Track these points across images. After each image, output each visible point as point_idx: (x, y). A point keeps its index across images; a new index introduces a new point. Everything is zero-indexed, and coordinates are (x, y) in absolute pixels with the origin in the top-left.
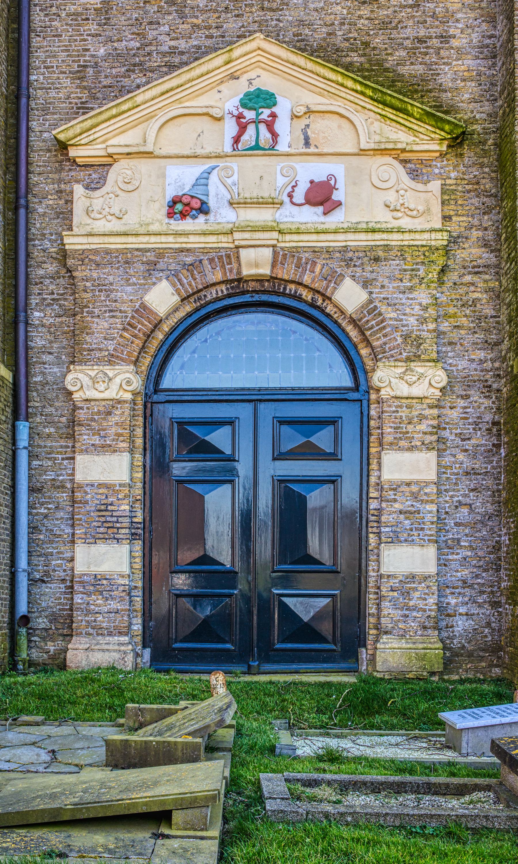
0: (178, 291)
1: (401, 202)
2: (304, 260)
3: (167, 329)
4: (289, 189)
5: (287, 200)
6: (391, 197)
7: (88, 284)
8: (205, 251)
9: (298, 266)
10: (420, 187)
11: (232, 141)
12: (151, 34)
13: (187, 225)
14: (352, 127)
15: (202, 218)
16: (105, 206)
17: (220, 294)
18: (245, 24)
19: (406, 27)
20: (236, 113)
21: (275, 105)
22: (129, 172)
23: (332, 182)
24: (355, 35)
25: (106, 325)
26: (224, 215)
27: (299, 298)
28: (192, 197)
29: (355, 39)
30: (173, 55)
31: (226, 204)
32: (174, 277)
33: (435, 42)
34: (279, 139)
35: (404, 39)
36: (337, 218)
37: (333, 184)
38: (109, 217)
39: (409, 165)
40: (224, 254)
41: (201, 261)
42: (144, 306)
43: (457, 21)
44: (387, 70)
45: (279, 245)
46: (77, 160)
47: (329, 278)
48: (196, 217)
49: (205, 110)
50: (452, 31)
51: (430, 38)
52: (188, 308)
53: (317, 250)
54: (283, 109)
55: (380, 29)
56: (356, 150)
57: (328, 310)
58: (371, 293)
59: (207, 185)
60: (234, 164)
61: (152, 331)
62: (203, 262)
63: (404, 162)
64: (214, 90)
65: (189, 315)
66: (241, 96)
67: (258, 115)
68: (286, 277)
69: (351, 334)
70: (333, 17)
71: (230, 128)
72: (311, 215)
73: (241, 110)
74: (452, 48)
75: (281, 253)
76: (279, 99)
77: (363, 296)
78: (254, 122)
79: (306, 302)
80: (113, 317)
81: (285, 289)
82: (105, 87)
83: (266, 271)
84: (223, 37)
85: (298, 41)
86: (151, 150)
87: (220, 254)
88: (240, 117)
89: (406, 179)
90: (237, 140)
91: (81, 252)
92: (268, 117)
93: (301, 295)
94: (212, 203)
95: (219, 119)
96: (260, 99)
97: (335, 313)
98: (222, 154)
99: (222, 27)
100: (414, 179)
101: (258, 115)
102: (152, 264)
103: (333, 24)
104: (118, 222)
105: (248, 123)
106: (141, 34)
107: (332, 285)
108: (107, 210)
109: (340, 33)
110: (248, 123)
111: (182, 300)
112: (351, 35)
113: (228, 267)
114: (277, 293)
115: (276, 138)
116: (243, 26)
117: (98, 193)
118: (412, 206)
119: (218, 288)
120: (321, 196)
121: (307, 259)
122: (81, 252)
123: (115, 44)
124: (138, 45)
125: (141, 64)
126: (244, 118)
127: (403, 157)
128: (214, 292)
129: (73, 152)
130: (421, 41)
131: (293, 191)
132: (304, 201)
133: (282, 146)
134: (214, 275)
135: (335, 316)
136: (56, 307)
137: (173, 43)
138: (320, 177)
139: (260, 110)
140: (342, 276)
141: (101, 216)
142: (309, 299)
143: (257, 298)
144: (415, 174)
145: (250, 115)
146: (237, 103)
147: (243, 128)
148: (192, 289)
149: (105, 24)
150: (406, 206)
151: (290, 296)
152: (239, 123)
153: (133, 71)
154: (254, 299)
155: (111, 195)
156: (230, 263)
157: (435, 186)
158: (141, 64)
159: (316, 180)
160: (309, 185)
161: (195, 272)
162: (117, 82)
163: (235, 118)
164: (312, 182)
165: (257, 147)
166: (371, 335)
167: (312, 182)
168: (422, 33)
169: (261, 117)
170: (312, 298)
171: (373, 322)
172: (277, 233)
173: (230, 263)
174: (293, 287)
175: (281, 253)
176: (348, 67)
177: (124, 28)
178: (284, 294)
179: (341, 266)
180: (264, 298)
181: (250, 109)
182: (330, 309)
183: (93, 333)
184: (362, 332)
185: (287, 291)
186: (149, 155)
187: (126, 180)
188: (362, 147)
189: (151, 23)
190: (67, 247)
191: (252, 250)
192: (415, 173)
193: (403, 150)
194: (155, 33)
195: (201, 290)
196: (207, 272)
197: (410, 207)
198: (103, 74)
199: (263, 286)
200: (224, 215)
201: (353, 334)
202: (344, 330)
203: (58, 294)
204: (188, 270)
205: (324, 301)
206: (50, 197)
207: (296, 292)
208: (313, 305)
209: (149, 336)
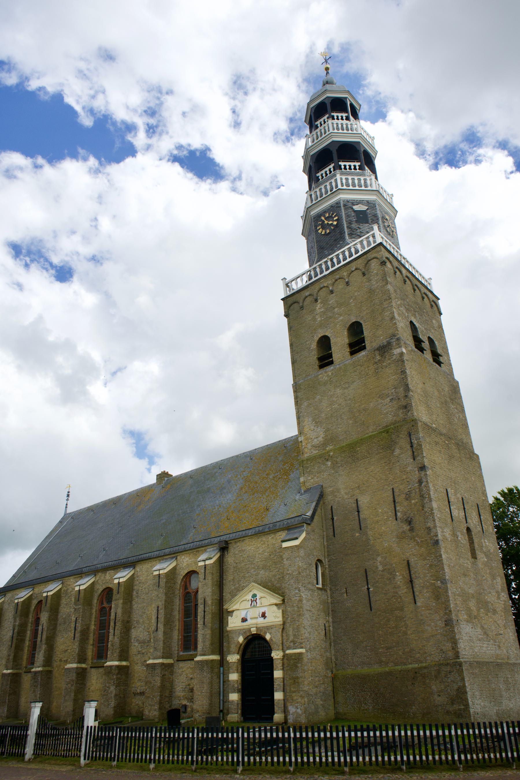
13: (245, 624)
102: (240, 632)
127: (276, 605)
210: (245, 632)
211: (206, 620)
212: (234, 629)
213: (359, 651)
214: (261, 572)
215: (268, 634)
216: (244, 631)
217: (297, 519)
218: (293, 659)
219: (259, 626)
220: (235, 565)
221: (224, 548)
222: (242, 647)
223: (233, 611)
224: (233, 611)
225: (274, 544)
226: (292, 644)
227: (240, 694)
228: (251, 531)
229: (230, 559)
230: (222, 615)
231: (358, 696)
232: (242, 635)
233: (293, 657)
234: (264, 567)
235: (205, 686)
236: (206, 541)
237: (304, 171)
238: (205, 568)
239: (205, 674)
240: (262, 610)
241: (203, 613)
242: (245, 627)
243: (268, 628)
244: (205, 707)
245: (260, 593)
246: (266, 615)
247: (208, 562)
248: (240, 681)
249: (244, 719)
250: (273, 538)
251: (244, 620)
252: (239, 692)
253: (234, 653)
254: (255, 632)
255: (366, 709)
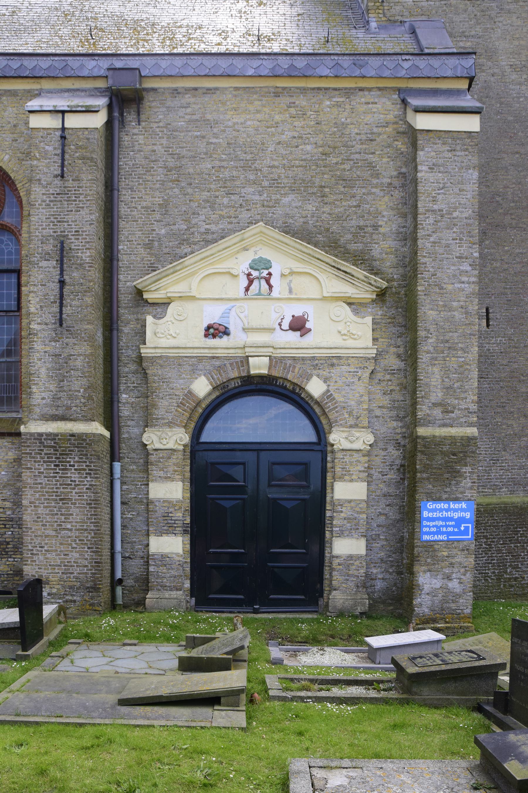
26: (237, 339)
72: (293, 337)
102: (195, 364)
210: (219, 369)
211: (67, 310)
212: (172, 353)
213: (506, 455)
214: (285, 200)
215: (315, 379)
216: (218, 363)
217: (453, 61)
218: (442, 453)
219: (280, 353)
220: (171, 163)
221: (125, 99)
222: (200, 410)
225: (345, 125)
226: (437, 412)
227: (188, 538)
228: (255, 63)
229: (139, 140)
230: (117, 311)
231: (499, 551)
232: (209, 375)
233: (445, 448)
234: (302, 187)
235: (74, 511)
236: (44, 63)
238: (63, 138)
239: (75, 476)
240: (298, 310)
241: (56, 286)
242: (220, 353)
244: (76, 571)
245: (284, 259)
246: (308, 325)
247: (73, 122)
248: (187, 504)
249: (197, 604)
250: (338, 105)
251: (215, 331)
252: (185, 532)
253: (170, 424)
254: (265, 371)
255: (516, 579)
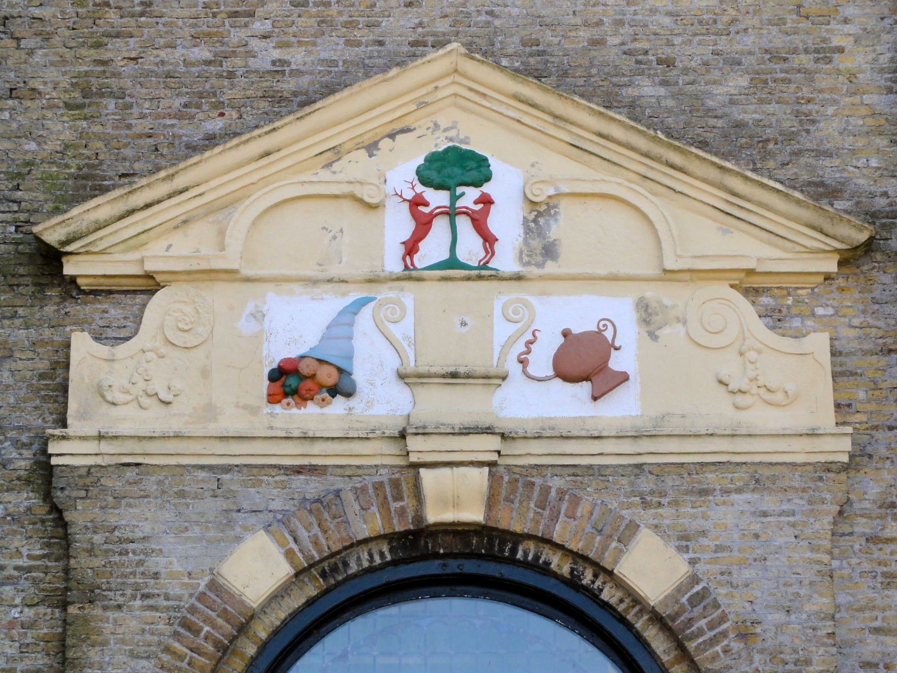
0: (289, 555)
1: (752, 374)
2: (553, 493)
3: (263, 635)
4: (520, 347)
5: (513, 368)
6: (730, 367)
7: (98, 539)
8: (347, 472)
9: (542, 505)
10: (787, 344)
11: (401, 250)
12: (236, 36)
13: (311, 416)
14: (611, 203)
15: (339, 405)
16: (137, 378)
17: (378, 560)
18: (425, 20)
19: (746, 30)
20: (409, 195)
21: (488, 179)
22: (188, 309)
23: (609, 334)
24: (646, 45)
25: (134, 624)
26: (380, 399)
27: (545, 570)
28: (320, 361)
29: (646, 53)
30: (278, 77)
31: (393, 377)
32: (279, 524)
33: (805, 60)
34: (497, 246)
35: (742, 53)
36: (622, 408)
37: (610, 339)
38: (145, 401)
39: (765, 300)
40: (385, 479)
41: (338, 493)
42: (214, 586)
43: (846, 21)
44: (709, 112)
45: (501, 461)
46: (80, 281)
47: (607, 530)
48: (329, 403)
49: (345, 189)
50: (836, 42)
51: (795, 51)
52: (311, 591)
53: (579, 472)
54: (506, 186)
55: (696, 35)
56: (653, 271)
57: (605, 596)
58: (693, 562)
59: (350, 338)
60: (409, 296)
61: (233, 639)
62: (343, 495)
63: (751, 292)
64: (367, 148)
65: (310, 603)
66: (421, 161)
67: (454, 198)
68: (517, 528)
69: (654, 645)
70: (599, 9)
71: (401, 226)
72: (569, 403)
73: (420, 188)
74: (839, 72)
75: (506, 478)
76: (495, 165)
77: (680, 568)
78: (447, 213)
79: (555, 575)
80: (152, 608)
81: (514, 550)
82: (140, 136)
83: (474, 514)
84: (381, 43)
85: (531, 55)
86: (235, 266)
87: (377, 479)
88: (416, 203)
89: (758, 327)
90: (411, 248)
91: (83, 472)
92: (476, 202)
93: (547, 564)
94: (359, 375)
95: (372, 207)
96: (457, 168)
97: (621, 601)
98: (382, 275)
99: (378, 25)
100: (772, 328)
101: (454, 198)
102: (223, 487)
103: (600, 23)
104: (162, 410)
105: (432, 216)
106: (216, 34)
107: (614, 544)
108: (141, 385)
109: (617, 40)
110: (432, 216)
111: (297, 575)
112: (637, 45)
113: (395, 505)
114: (491, 557)
115: (492, 246)
116: (420, 24)
117: (122, 350)
118: (772, 385)
119: (375, 547)
120: (585, 363)
121: (561, 493)
122: (83, 472)
123: (162, 54)
124: (207, 55)
125: (215, 95)
126: (426, 204)
127: (750, 284)
128: (365, 556)
129: (69, 269)
130: (774, 55)
131: (528, 352)
132: (551, 373)
133: (506, 260)
134: (365, 522)
135: (621, 608)
136: (24, 584)
137: (276, 54)
138: (583, 324)
139: (460, 190)
140: (633, 527)
141: (128, 398)
142: (565, 570)
143: (453, 566)
144: (775, 318)
145: (437, 199)
146: (412, 176)
147: (423, 225)
148: (320, 551)
149: (142, 14)
150: (760, 383)
151: (525, 564)
152: (415, 215)
153: (199, 106)
154: (448, 571)
155: (150, 355)
156: (398, 497)
157: (818, 343)
158: (215, 95)
159: (576, 330)
160: (561, 340)
161: (326, 515)
162: (165, 126)
163: (407, 205)
164: (566, 334)
165: (452, 263)
166: (697, 647)
167: (566, 334)
168: (779, 41)
169: (460, 203)
170: (572, 570)
171: (703, 623)
172: (499, 438)
173: (398, 497)
174: (531, 546)
175: (506, 478)
176: (633, 109)
177: (180, 23)
178: (512, 561)
179: (629, 506)
180: (470, 567)
181: (439, 187)
182: (609, 594)
183: (105, 643)
184: (680, 646)
185: (519, 555)
186: (230, 275)
187: (181, 325)
188: (670, 265)
189: (235, 14)
190: (54, 461)
191: (446, 471)
192: (777, 315)
193: (750, 272)
194: (243, 34)
195: (339, 552)
196: (351, 516)
197: (769, 385)
198: (135, 111)
199: (469, 544)
200: (380, 399)
201: (660, 644)
202: (638, 637)
203: (30, 557)
204: (310, 511)
205: (596, 576)
206: (17, 355)
207: (537, 557)
208: (573, 582)
209: (225, 649)
223: (149, 285)
224: (149, 285)
237: (281, 361)
240: (581, 312)
243: (671, 483)
